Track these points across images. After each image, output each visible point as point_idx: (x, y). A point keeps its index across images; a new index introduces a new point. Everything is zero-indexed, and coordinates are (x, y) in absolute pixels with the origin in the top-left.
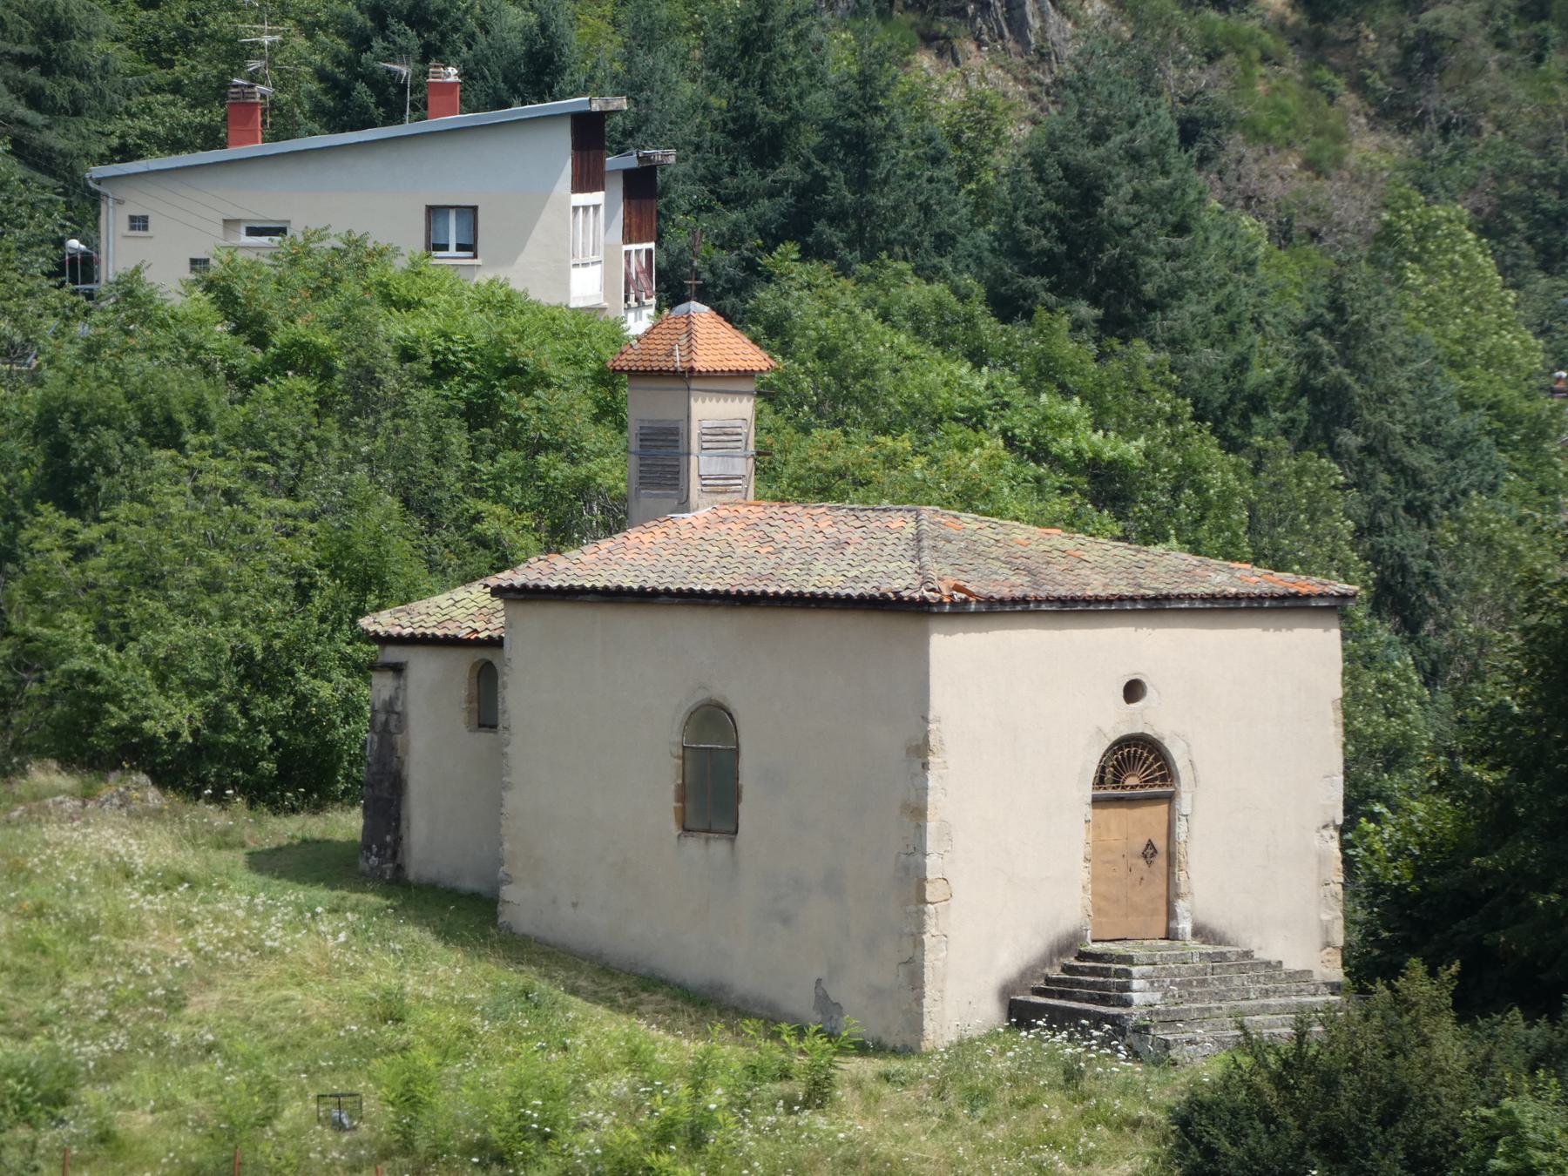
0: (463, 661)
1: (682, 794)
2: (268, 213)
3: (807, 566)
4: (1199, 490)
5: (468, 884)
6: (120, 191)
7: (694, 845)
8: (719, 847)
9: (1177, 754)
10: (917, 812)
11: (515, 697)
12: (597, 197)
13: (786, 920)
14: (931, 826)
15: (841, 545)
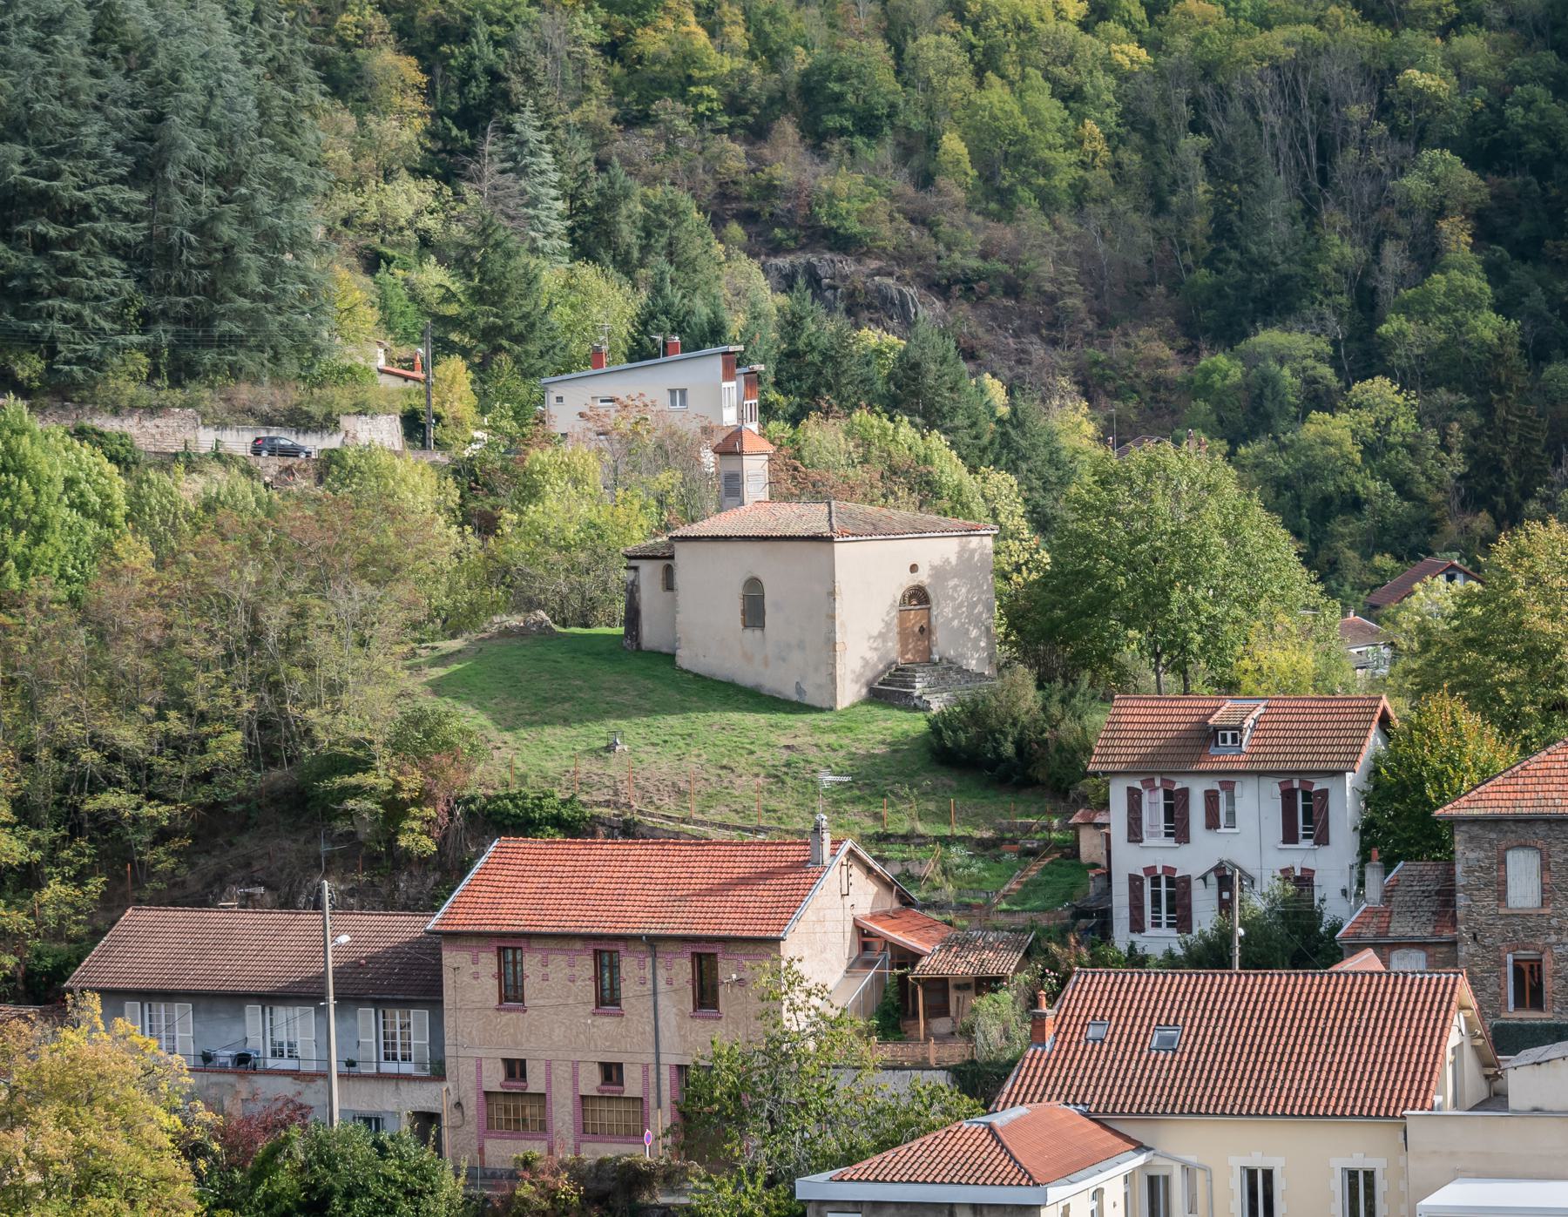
0: (661, 564)
1: (744, 613)
2: (608, 394)
3: (788, 525)
4: (1029, 611)
5: (665, 650)
6: (551, 388)
7: (748, 632)
8: (758, 633)
9: (932, 595)
10: (832, 617)
11: (680, 578)
12: (733, 384)
13: (784, 660)
14: (837, 623)
15: (801, 516)
